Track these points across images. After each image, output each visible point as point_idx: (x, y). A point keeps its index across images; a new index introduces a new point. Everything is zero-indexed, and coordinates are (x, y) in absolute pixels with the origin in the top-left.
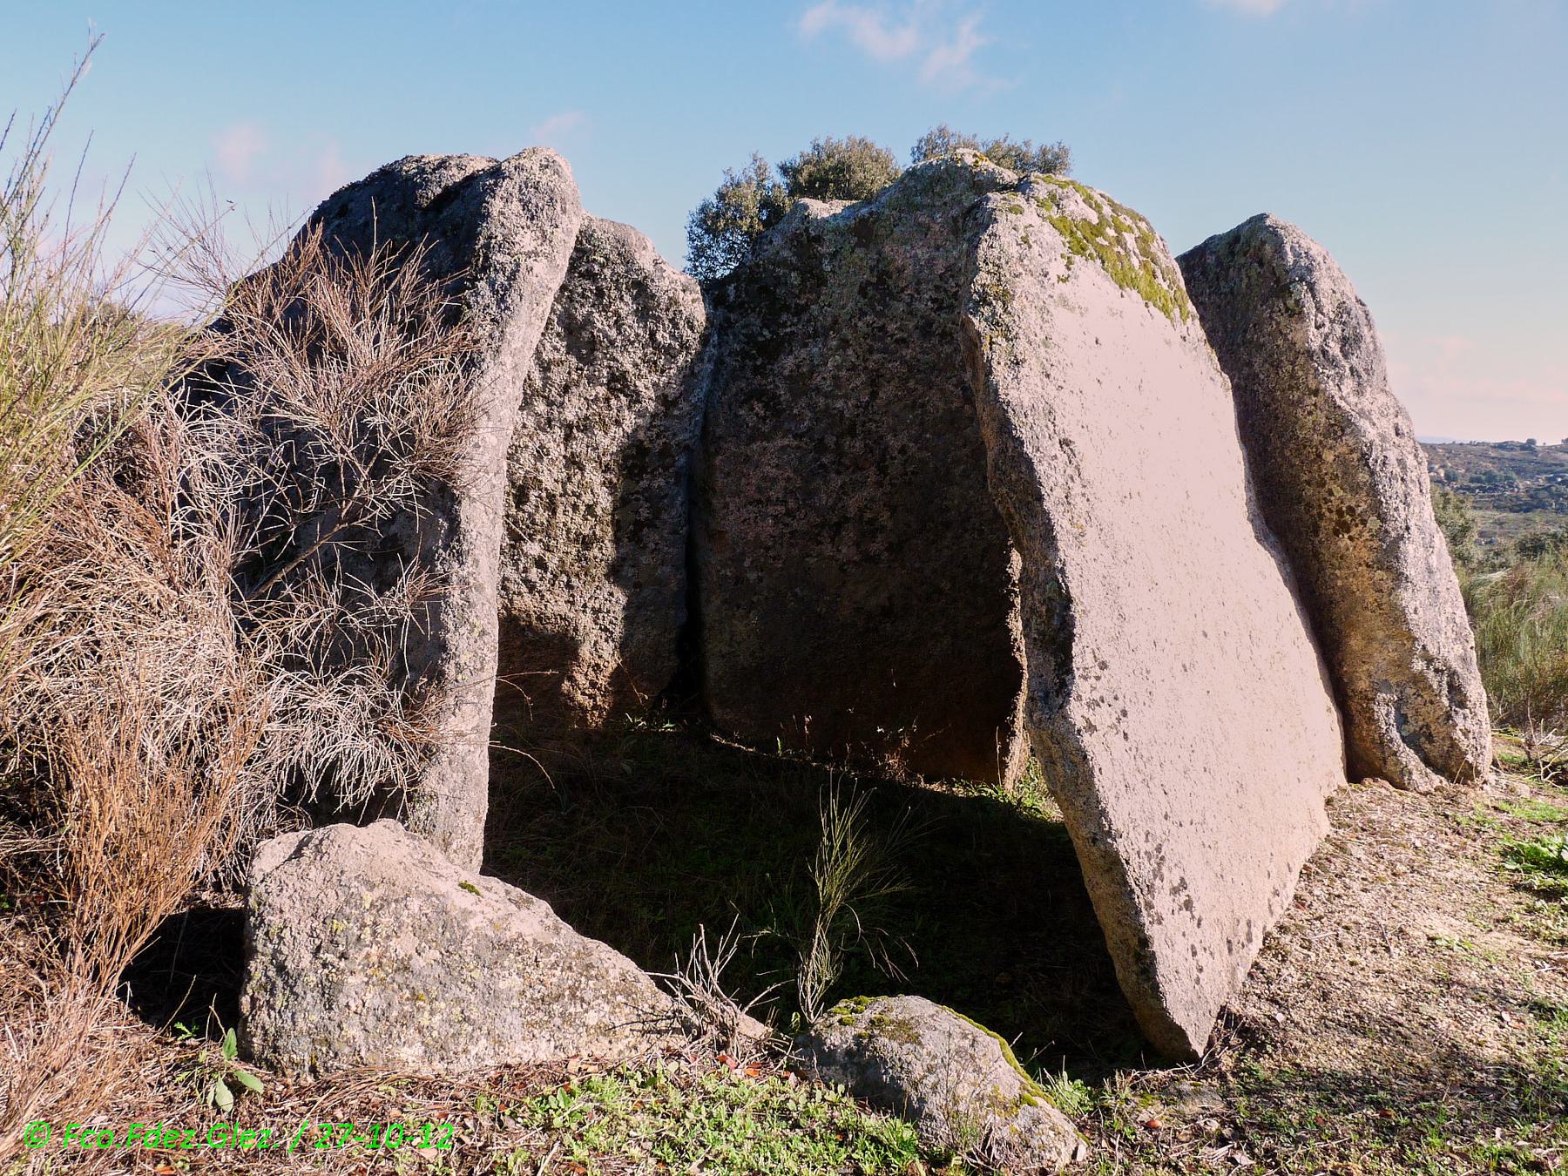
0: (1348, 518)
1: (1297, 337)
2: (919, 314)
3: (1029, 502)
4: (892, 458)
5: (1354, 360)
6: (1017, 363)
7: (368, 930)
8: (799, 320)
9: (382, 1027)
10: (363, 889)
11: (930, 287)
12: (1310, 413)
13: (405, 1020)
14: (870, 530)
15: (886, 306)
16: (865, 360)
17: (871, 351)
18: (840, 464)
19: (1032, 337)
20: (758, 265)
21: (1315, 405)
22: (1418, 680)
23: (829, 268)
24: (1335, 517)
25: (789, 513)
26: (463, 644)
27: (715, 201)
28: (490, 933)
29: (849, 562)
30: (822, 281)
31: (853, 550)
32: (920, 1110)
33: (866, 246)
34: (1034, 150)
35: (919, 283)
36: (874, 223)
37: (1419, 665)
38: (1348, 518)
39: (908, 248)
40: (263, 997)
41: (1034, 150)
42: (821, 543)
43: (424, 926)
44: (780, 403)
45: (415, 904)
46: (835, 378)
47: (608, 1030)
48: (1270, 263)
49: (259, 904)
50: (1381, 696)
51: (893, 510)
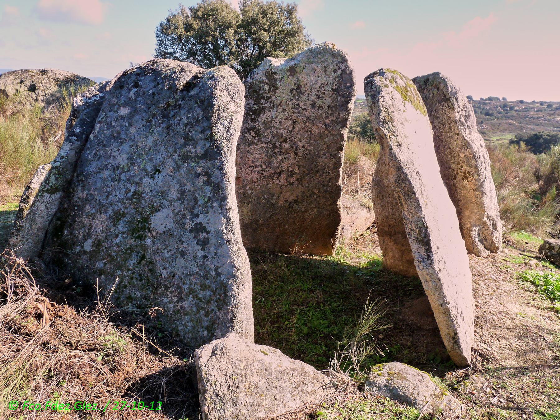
0: (468, 175)
1: (452, 116)
2: (311, 100)
3: (409, 194)
4: (299, 149)
5: (468, 123)
6: (400, 145)
7: (244, 377)
8: (268, 102)
9: (253, 408)
10: (240, 363)
11: (316, 90)
12: (455, 141)
13: (259, 404)
14: (291, 174)
15: (299, 97)
16: (291, 116)
17: (293, 113)
18: (281, 152)
19: (402, 135)
20: (253, 82)
21: (457, 138)
22: (485, 223)
23: (279, 84)
24: (463, 174)
25: (263, 170)
26: (241, 265)
27: (165, 22)
28: (279, 369)
29: (283, 185)
30: (276, 88)
31: (285, 181)
32: (416, 403)
33: (293, 76)
34: (285, 6)
35: (311, 89)
36: (296, 68)
37: (485, 219)
38: (468, 175)
39: (308, 77)
40: (212, 406)
41: (285, 6)
42: (274, 179)
43: (260, 371)
44: (260, 132)
45: (256, 364)
46: (280, 122)
47: (314, 392)
48: (442, 90)
49: (206, 375)
50: (474, 228)
51: (299, 167)
